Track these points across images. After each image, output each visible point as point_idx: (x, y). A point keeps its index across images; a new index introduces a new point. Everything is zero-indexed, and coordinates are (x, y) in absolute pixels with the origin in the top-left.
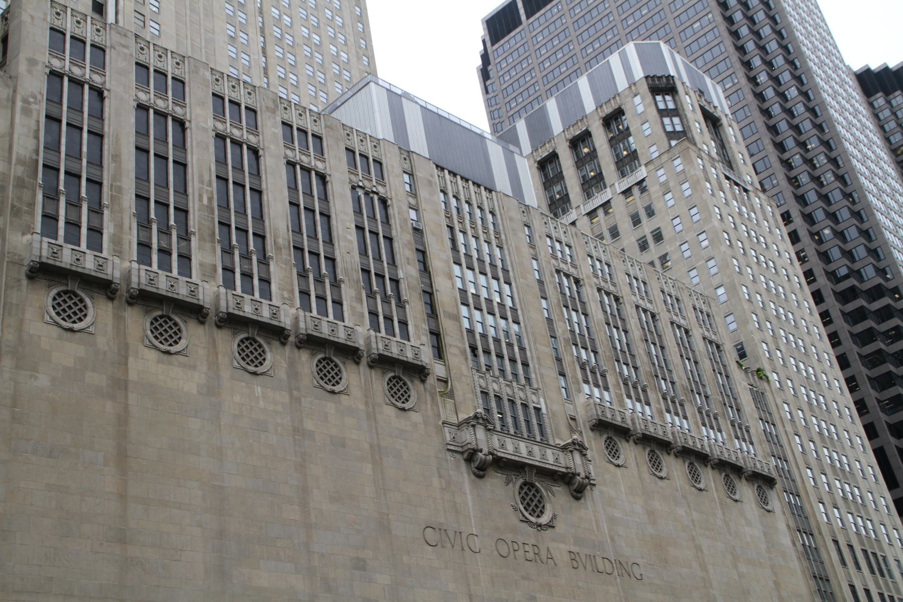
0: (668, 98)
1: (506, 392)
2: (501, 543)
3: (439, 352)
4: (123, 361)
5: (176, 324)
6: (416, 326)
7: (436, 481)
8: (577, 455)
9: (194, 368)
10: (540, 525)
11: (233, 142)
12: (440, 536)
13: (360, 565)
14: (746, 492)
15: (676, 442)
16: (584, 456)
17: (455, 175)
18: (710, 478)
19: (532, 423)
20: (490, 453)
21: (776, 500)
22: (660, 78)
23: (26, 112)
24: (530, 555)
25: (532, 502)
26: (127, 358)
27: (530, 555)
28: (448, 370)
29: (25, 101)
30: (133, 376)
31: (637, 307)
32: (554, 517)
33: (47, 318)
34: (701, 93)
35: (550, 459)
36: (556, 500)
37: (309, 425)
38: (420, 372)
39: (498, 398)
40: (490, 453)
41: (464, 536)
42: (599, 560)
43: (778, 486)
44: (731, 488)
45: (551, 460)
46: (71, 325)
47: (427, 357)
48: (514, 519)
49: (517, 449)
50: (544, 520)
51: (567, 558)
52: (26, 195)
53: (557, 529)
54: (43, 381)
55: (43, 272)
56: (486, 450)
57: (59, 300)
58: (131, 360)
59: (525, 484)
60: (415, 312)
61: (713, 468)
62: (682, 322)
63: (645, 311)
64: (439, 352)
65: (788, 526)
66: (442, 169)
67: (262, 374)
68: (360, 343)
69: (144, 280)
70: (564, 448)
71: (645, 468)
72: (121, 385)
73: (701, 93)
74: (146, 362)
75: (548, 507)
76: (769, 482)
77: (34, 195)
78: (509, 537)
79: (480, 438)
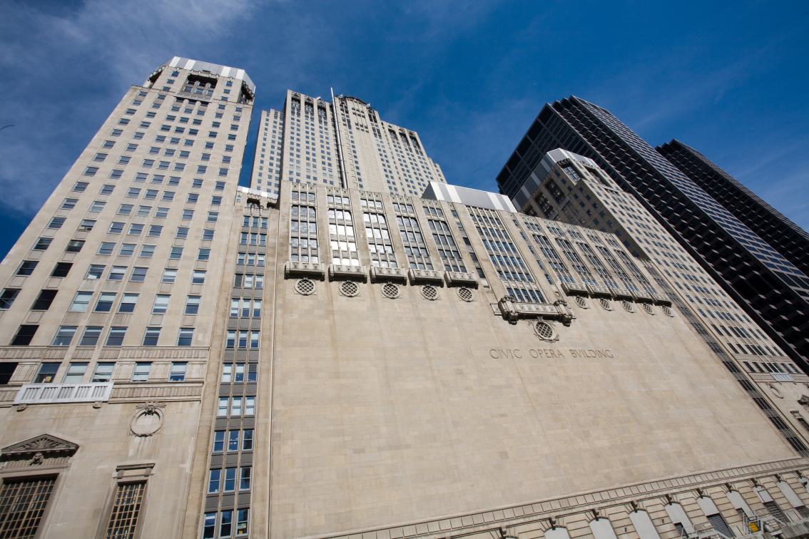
0: (569, 168)
1: (520, 286)
2: (532, 352)
3: (482, 276)
4: (331, 301)
5: (395, 287)
6: (469, 267)
7: (492, 329)
8: (562, 306)
9: (364, 301)
10: (551, 340)
11: (435, 221)
12: (496, 353)
13: (460, 372)
14: (657, 309)
15: (590, 291)
16: (565, 305)
17: (476, 208)
18: (616, 305)
19: (538, 297)
20: (516, 312)
21: (673, 310)
22: (564, 161)
23: (283, 220)
24: (550, 355)
25: (545, 332)
26: (332, 301)
27: (550, 355)
28: (488, 281)
29: (283, 216)
30: (336, 307)
31: (534, 235)
32: (558, 336)
33: (296, 292)
34: (584, 163)
35: (549, 310)
36: (557, 326)
37: (423, 315)
38: (474, 285)
39: (516, 289)
40: (516, 312)
41: (512, 352)
42: (587, 352)
43: (673, 305)
44: (582, 304)
45: (549, 310)
46: (306, 293)
47: (475, 277)
48: (537, 340)
49: (530, 308)
50: (553, 337)
51: (569, 353)
52: (285, 248)
53: (561, 340)
54: (295, 316)
55: (291, 275)
56: (514, 311)
57: (301, 284)
58: (334, 302)
59: (539, 323)
60: (467, 261)
61: (592, 298)
62: (602, 245)
63: (539, 236)
64: (482, 276)
65: (685, 322)
66: (476, 208)
67: (356, 296)
68: (442, 277)
69: (416, 274)
70: (555, 304)
71: (600, 308)
72: (330, 313)
73: (584, 163)
74: (342, 302)
75: (553, 331)
76: (669, 304)
77: (288, 248)
78: (536, 349)
79: (509, 306)
